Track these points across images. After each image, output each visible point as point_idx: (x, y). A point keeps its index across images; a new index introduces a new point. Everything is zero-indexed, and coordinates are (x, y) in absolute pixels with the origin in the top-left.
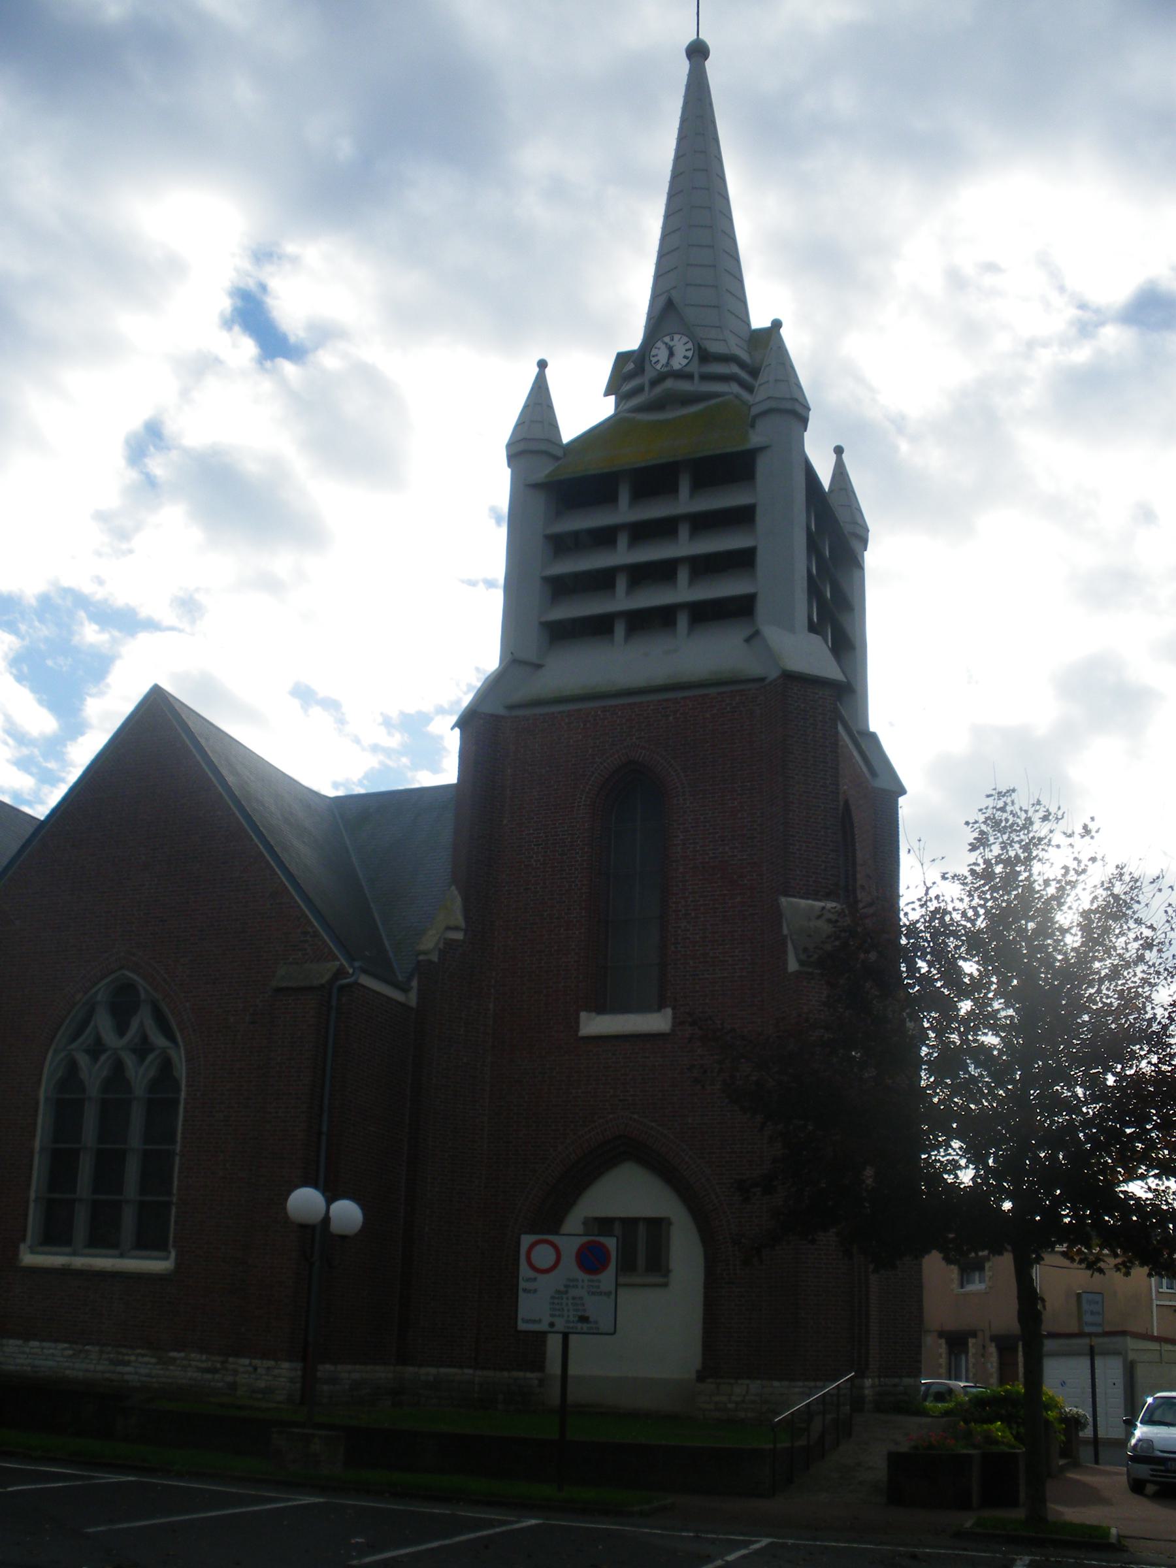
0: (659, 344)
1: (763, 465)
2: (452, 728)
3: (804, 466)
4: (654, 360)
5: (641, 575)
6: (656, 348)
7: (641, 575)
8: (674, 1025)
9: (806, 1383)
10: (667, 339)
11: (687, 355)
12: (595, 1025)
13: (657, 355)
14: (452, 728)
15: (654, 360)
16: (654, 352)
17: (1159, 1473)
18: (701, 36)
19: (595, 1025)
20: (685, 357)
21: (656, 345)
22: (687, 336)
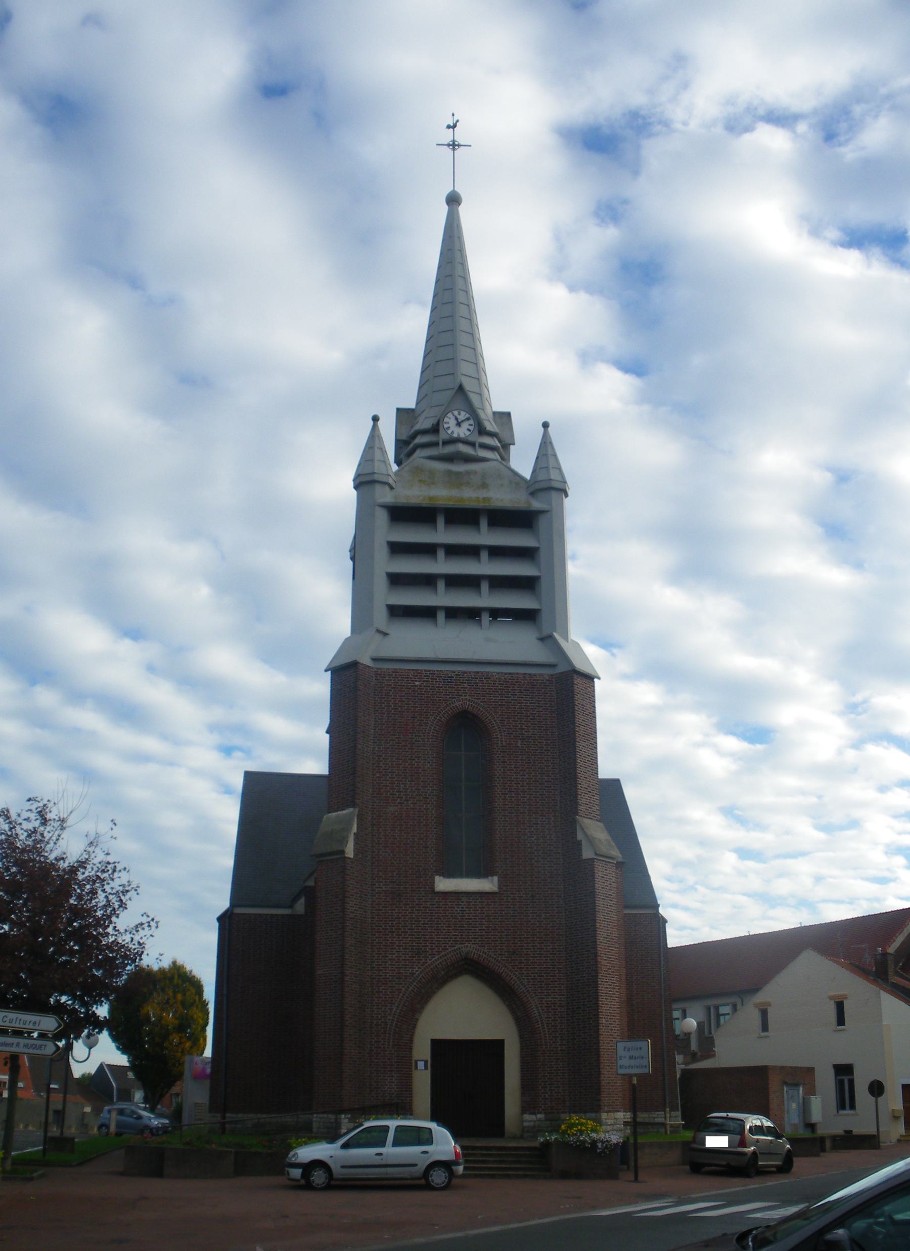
0: (450, 415)
1: (542, 522)
2: (326, 671)
3: (425, 460)
4: (446, 426)
5: (455, 582)
6: (447, 417)
7: (455, 582)
8: (500, 887)
9: (318, 1115)
10: (456, 413)
11: (471, 429)
12: (443, 884)
13: (448, 423)
14: (326, 671)
15: (446, 426)
16: (446, 420)
17: (520, 1173)
18: (455, 189)
19: (443, 884)
20: (469, 430)
21: (447, 415)
22: (464, 411)
